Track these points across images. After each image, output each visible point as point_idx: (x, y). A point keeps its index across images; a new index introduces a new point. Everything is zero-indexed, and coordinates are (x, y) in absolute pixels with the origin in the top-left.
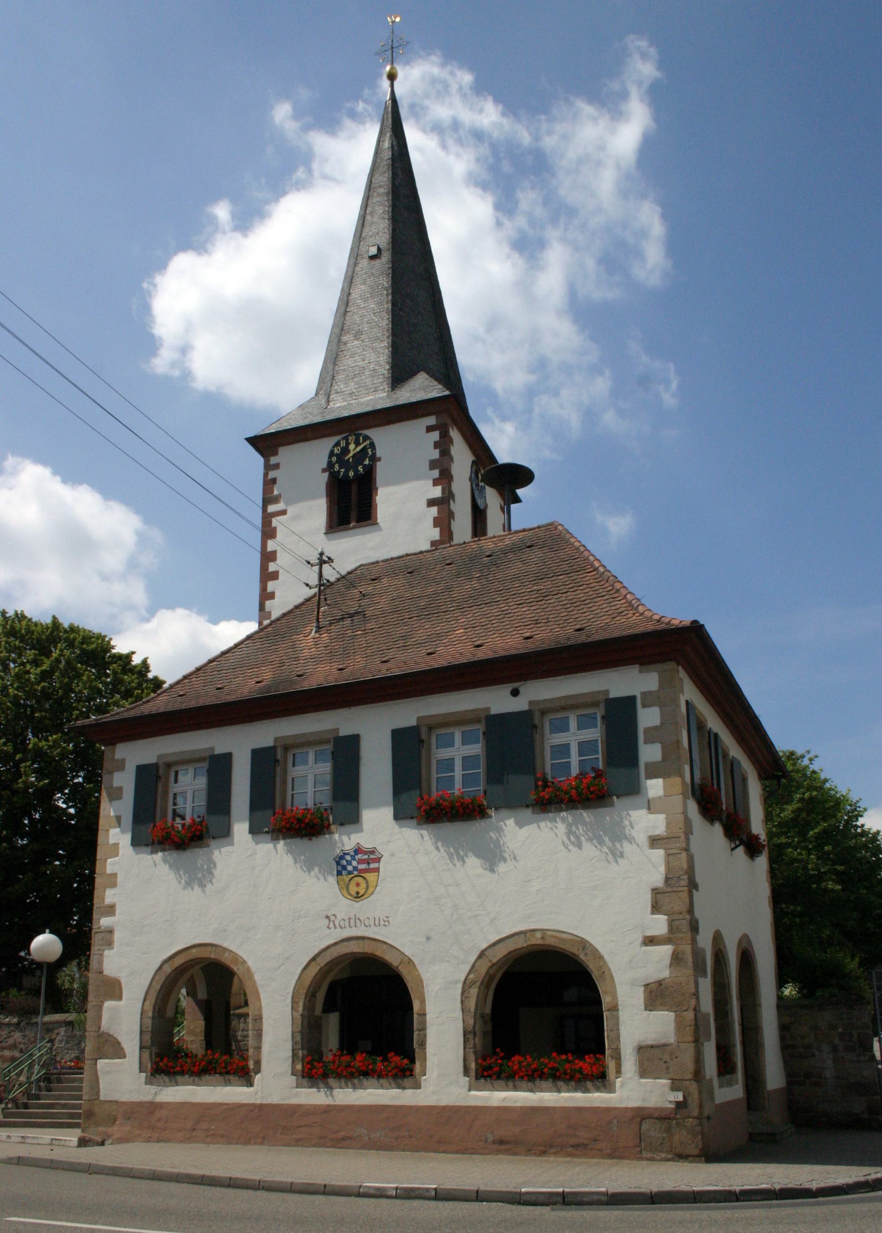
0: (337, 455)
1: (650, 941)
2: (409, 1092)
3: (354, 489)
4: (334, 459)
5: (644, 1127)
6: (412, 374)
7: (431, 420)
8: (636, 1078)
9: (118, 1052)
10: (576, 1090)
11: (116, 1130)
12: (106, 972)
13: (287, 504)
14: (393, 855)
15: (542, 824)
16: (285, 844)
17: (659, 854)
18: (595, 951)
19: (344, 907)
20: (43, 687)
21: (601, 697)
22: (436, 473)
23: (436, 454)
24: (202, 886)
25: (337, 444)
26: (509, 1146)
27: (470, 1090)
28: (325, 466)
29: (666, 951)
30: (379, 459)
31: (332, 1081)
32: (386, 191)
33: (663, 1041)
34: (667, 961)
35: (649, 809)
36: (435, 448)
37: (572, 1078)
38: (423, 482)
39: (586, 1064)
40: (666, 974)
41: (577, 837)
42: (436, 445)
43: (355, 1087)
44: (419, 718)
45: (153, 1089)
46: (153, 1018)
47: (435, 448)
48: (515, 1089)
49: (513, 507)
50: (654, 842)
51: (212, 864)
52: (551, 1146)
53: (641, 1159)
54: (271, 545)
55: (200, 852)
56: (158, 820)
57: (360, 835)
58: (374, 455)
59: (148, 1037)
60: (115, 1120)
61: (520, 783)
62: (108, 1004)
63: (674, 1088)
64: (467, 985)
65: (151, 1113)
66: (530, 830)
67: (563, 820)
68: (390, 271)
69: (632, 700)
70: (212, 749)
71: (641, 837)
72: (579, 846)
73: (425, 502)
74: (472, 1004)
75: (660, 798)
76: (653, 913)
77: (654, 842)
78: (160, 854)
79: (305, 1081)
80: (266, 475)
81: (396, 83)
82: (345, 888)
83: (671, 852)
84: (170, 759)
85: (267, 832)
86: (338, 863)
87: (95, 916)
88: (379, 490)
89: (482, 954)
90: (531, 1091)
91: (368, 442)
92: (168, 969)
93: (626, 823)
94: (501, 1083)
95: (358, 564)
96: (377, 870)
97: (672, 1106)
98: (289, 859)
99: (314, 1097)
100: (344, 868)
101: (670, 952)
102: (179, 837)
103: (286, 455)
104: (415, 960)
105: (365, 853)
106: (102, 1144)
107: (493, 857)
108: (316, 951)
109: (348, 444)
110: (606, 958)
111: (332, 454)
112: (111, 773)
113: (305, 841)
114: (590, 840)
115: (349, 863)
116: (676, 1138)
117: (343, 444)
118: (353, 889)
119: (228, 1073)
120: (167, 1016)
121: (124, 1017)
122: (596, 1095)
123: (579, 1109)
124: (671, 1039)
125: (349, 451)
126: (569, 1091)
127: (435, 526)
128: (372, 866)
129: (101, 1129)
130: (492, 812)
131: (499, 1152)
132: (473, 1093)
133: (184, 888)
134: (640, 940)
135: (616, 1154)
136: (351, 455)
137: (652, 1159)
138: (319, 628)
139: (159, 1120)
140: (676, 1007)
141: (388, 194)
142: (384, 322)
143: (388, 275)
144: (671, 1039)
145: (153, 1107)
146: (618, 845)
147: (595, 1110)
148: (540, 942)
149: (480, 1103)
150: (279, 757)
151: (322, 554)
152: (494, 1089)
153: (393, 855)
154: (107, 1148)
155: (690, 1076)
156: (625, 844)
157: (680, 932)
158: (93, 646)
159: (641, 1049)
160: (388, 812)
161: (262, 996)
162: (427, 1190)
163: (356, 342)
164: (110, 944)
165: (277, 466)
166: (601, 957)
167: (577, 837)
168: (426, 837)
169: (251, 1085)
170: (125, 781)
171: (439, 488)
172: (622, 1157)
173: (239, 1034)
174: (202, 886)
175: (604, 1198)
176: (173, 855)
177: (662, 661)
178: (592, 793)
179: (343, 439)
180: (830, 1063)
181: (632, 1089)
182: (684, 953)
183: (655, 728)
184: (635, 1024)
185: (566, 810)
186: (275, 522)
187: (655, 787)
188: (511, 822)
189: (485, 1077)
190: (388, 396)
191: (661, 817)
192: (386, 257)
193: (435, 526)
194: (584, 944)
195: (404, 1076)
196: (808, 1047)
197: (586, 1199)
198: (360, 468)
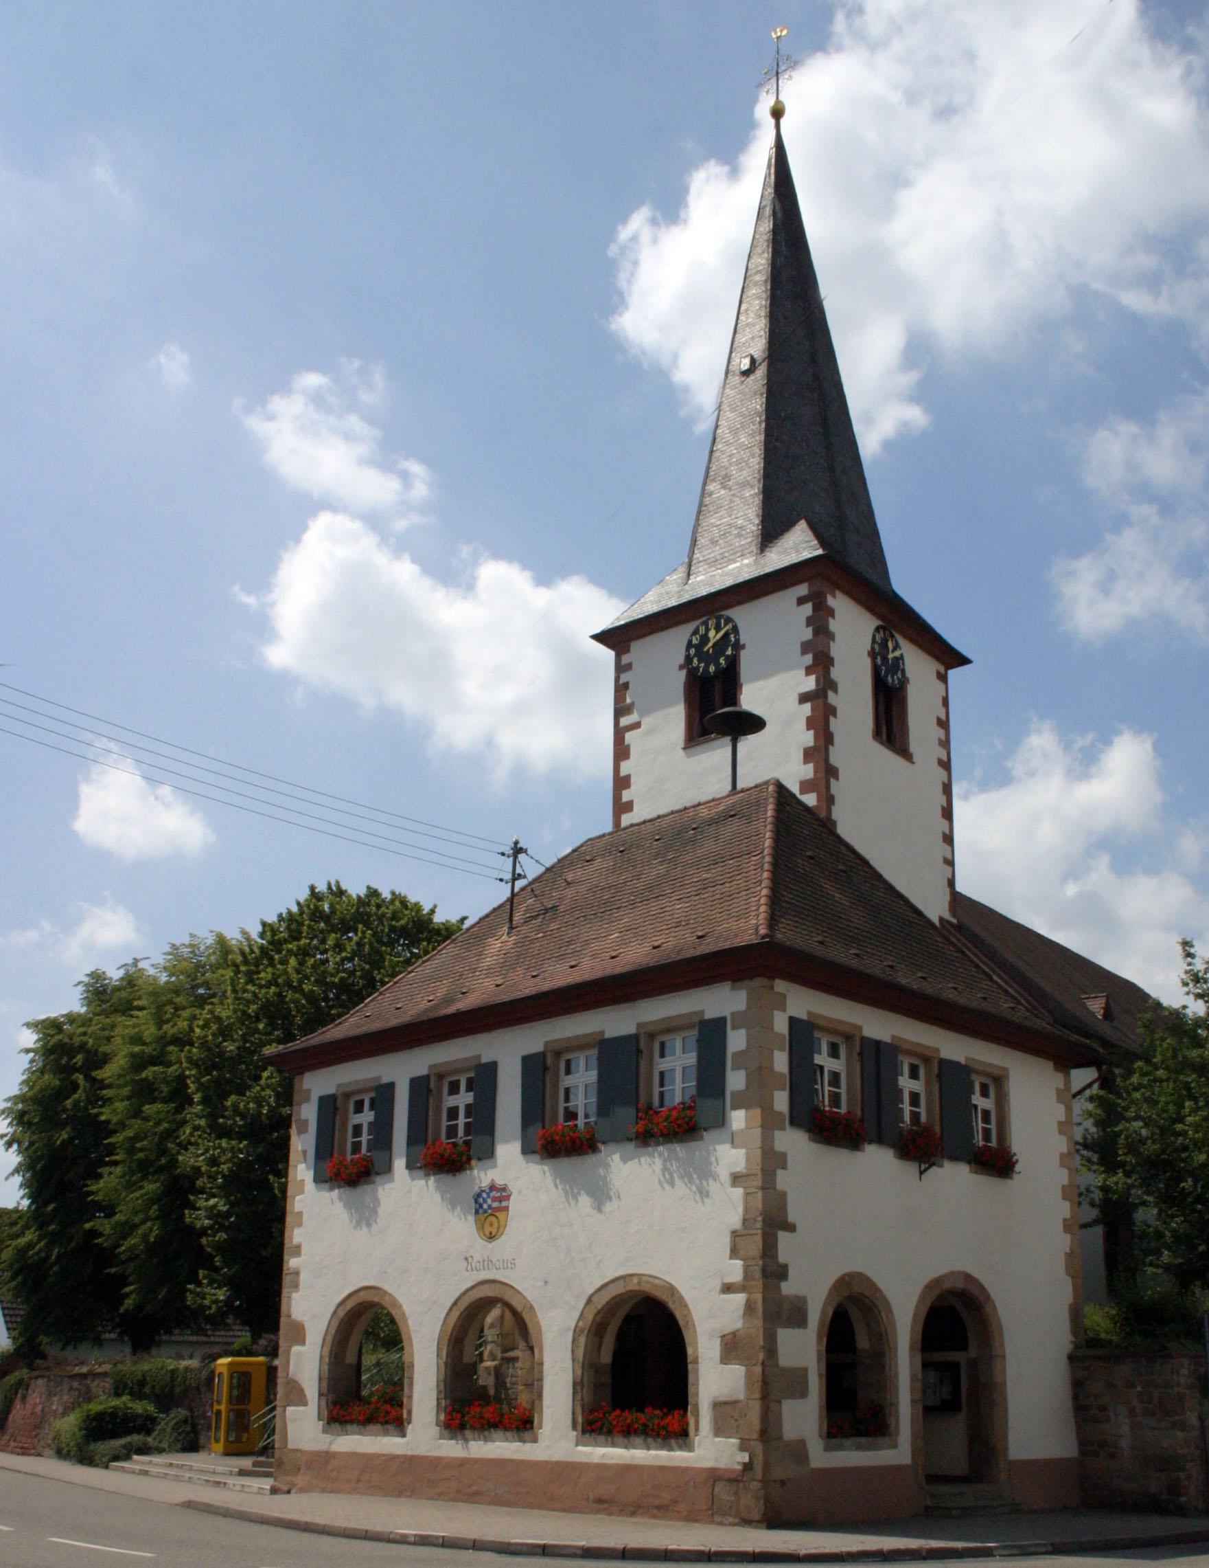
0: (695, 646)
1: (728, 1288)
2: (528, 1445)
3: (718, 687)
4: (692, 651)
5: (717, 1490)
6: (788, 526)
7: (803, 590)
8: (711, 1436)
9: (303, 1401)
10: (662, 1448)
11: (300, 1480)
12: (293, 1316)
13: (642, 715)
14: (520, 1192)
15: (643, 1160)
16: (436, 1181)
17: (739, 1192)
18: (681, 1298)
19: (480, 1248)
20: (342, 979)
21: (696, 1020)
22: (808, 659)
23: (808, 634)
24: (369, 1225)
25: (696, 632)
26: (606, 1506)
27: (577, 1445)
28: (681, 660)
29: (739, 1299)
30: (743, 647)
31: (468, 1433)
32: (764, 278)
33: (733, 1399)
34: (741, 1312)
35: (732, 1143)
36: (808, 625)
37: (658, 1435)
38: (794, 672)
39: (672, 1420)
40: (739, 1325)
41: (671, 1175)
42: (809, 621)
43: (486, 1440)
44: (546, 1043)
45: (328, 1437)
46: (330, 1364)
47: (808, 625)
48: (614, 1445)
49: (953, 674)
50: (736, 1179)
51: (376, 1201)
52: (640, 1507)
53: (713, 1522)
54: (626, 768)
55: (368, 1188)
56: (336, 1155)
57: (495, 1171)
58: (737, 641)
59: (325, 1384)
60: (299, 1469)
61: (625, 1114)
62: (296, 1349)
63: (742, 1448)
64: (577, 1332)
65: (327, 1462)
66: (632, 1165)
67: (660, 1155)
68: (764, 390)
69: (722, 1020)
70: (379, 1078)
71: (724, 1174)
72: (672, 1184)
73: (795, 698)
74: (580, 1353)
75: (742, 1131)
76: (731, 1258)
77: (736, 1179)
78: (337, 1191)
79: (446, 1433)
80: (617, 679)
81: (782, 121)
82: (480, 1227)
83: (749, 1190)
84: (349, 1089)
85: (420, 1168)
86: (476, 1201)
87: (286, 1257)
88: (744, 689)
89: (589, 1301)
90: (626, 1447)
91: (730, 625)
92: (341, 1313)
93: (713, 1159)
94: (601, 1438)
95: (585, 839)
96: (506, 1209)
97: (740, 1467)
98: (437, 1197)
99: (452, 1449)
100: (481, 1206)
101: (743, 1302)
102: (352, 1172)
103: (640, 650)
104: (535, 1306)
105: (498, 1190)
106: (289, 1492)
107: (601, 1195)
108: (457, 1295)
109: (707, 630)
110: (691, 1307)
111: (690, 645)
112: (299, 1104)
113: (451, 1176)
114: (681, 1177)
115: (485, 1201)
116: (742, 1501)
117: (702, 630)
118: (487, 1229)
119: (387, 1422)
120: (347, 1362)
121: (305, 1363)
122: (679, 1453)
123: (662, 1469)
124: (742, 1397)
125: (708, 640)
126: (656, 1449)
127: (808, 729)
128: (504, 1204)
129: (289, 1478)
130: (602, 1147)
131: (599, 1511)
132: (580, 1448)
133: (355, 1228)
134: (719, 1288)
135: (691, 1517)
136: (710, 644)
137: (721, 1524)
138: (511, 928)
139: (333, 1470)
140: (745, 1360)
141: (766, 281)
142: (756, 462)
143: (762, 394)
144: (742, 1397)
145: (328, 1456)
146: (705, 1184)
147: (675, 1469)
148: (636, 1288)
149: (584, 1460)
150: (432, 1086)
151: (516, 843)
152: (597, 1445)
153: (520, 1192)
154: (294, 1497)
155: (755, 1436)
156: (711, 1181)
157: (753, 1279)
158: (403, 922)
159: (717, 1406)
160: (516, 1146)
161: (414, 1342)
162: (437, 1537)
163: (723, 492)
164: (296, 1286)
165: (629, 667)
166: (686, 1306)
167: (671, 1175)
168: (548, 1174)
169: (403, 1435)
170: (308, 1112)
171: (813, 678)
172: (696, 1521)
173: (508, 1380)
174: (369, 1225)
175: (579, 1552)
176: (347, 1192)
177: (751, 978)
178: (679, 1126)
179: (703, 624)
180: (1126, 1429)
181: (711, 1449)
182: (756, 1303)
183: (742, 1052)
184: (715, 1379)
185: (663, 1144)
186: (629, 737)
187: (738, 1119)
188: (616, 1157)
189: (592, 1431)
190: (756, 562)
191: (741, 1152)
192: (761, 372)
193: (808, 729)
194: (672, 1290)
195: (526, 1429)
196: (1103, 1409)
197: (563, 1552)
198: (722, 661)
